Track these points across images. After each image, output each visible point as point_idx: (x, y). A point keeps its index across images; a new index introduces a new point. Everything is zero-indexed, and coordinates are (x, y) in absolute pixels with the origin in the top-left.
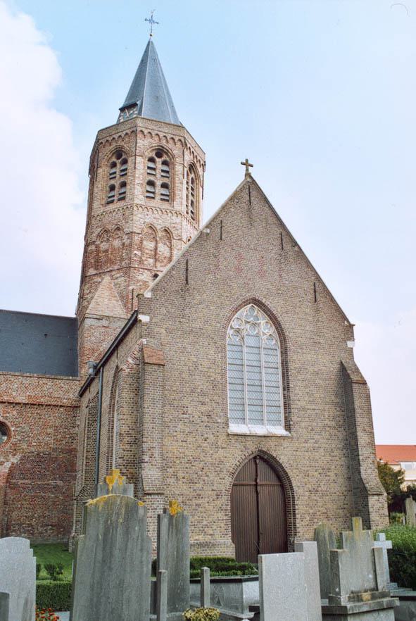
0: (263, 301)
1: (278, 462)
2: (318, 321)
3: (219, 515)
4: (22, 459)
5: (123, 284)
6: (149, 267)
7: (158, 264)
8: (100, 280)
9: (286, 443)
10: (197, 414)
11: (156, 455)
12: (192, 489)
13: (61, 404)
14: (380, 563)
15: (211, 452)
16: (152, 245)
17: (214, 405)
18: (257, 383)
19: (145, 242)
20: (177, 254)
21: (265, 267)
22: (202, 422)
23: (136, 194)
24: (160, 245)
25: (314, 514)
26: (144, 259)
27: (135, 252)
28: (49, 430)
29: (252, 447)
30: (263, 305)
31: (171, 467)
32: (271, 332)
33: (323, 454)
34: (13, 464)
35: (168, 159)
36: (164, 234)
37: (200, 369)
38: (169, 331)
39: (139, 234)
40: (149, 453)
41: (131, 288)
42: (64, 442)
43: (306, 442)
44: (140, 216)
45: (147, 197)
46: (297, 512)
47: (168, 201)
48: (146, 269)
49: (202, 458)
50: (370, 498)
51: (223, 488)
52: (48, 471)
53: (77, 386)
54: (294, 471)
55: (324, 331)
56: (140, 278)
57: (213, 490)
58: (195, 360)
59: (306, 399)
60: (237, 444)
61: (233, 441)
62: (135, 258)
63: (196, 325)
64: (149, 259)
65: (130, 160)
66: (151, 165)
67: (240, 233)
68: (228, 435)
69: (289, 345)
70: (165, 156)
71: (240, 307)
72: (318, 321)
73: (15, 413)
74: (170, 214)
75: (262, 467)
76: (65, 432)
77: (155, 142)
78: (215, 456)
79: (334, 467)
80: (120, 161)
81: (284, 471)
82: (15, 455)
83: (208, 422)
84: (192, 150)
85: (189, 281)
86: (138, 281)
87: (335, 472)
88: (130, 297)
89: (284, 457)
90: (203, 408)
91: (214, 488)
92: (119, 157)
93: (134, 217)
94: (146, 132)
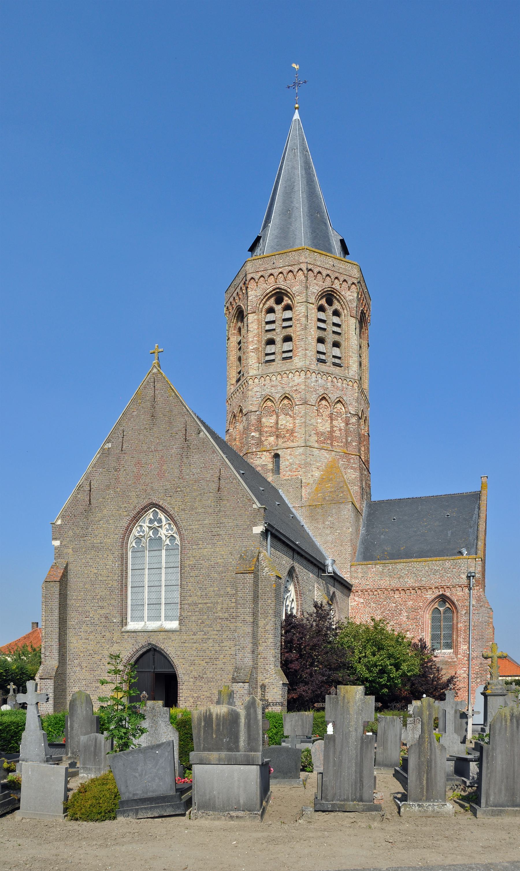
0: (160, 504)
2: (219, 511)
9: (174, 637)
10: (96, 617)
14: (488, 768)
15: (108, 646)
17: (111, 608)
18: (157, 584)
19: (264, 420)
22: (101, 623)
23: (251, 363)
25: (198, 697)
26: (263, 439)
27: (253, 434)
29: (142, 641)
31: (77, 659)
33: (211, 645)
35: (289, 302)
38: (75, 550)
39: (256, 411)
43: (194, 634)
44: (256, 389)
48: (264, 451)
49: (100, 652)
57: (108, 676)
58: (96, 571)
59: (198, 594)
60: (129, 639)
61: (126, 637)
62: (252, 442)
67: (141, 437)
70: (286, 298)
71: (137, 518)
72: (219, 511)
77: (269, 286)
79: (222, 656)
83: (106, 622)
87: (224, 661)
90: (102, 612)
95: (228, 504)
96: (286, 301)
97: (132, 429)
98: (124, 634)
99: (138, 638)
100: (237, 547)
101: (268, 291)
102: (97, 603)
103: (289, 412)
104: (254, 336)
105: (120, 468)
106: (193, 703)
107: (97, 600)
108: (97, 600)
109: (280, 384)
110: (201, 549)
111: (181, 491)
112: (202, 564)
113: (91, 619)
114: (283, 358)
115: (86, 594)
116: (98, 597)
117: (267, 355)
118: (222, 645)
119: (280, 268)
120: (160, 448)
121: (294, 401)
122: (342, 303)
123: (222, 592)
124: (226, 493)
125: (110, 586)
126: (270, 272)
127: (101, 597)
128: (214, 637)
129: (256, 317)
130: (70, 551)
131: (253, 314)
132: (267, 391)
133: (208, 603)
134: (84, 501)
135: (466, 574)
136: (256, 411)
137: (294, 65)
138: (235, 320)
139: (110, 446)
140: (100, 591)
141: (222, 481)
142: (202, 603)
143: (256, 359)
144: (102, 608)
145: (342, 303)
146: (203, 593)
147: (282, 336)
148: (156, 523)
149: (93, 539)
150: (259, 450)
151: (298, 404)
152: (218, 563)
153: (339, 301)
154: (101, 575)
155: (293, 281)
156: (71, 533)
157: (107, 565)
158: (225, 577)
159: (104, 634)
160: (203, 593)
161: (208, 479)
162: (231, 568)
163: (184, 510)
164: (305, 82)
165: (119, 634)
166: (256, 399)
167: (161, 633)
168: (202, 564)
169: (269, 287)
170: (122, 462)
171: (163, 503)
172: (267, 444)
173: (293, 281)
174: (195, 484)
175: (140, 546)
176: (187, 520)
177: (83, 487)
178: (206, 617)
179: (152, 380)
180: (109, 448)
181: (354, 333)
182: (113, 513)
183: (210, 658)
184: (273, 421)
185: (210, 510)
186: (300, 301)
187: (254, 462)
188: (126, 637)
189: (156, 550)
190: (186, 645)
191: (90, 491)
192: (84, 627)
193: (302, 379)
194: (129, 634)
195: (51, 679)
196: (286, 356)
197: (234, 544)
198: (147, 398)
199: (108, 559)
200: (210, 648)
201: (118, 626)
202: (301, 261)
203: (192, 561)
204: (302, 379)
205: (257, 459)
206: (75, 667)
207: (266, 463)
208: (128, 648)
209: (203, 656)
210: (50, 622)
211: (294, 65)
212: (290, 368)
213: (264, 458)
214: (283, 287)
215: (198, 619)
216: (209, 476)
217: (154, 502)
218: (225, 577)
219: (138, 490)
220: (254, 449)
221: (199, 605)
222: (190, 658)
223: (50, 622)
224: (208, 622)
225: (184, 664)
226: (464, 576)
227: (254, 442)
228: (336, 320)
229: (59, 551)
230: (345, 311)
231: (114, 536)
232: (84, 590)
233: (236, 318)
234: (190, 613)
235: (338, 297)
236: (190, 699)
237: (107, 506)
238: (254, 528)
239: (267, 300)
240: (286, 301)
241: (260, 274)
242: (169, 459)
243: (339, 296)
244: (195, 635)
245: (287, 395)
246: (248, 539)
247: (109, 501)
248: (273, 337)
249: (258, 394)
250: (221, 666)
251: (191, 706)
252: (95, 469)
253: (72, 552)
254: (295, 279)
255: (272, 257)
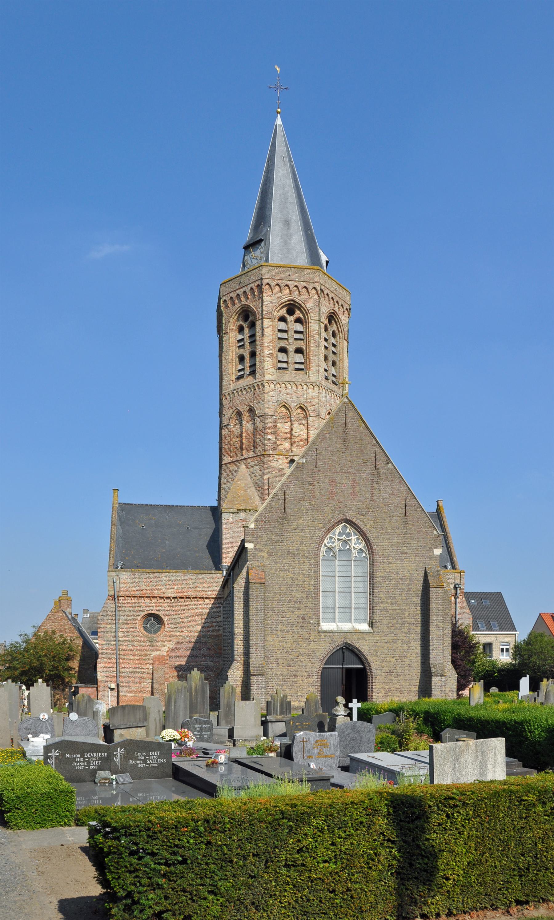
0: (354, 520)
1: (362, 653)
2: (406, 533)
3: (311, 689)
4: (176, 644)
5: (258, 473)
6: (284, 452)
7: (295, 448)
8: (236, 468)
9: (367, 637)
10: (293, 618)
11: (260, 648)
12: (289, 671)
13: (206, 596)
15: (305, 645)
16: (287, 426)
17: (308, 610)
19: (279, 425)
20: (313, 434)
21: (357, 489)
22: (298, 623)
23: (266, 367)
24: (296, 425)
25: (389, 689)
26: (278, 443)
27: (269, 437)
28: (198, 620)
29: (339, 641)
30: (354, 523)
31: (273, 656)
32: (361, 547)
33: (400, 645)
34: (169, 648)
35: (301, 316)
36: (299, 411)
37: (296, 582)
38: (270, 554)
39: (273, 416)
40: (255, 647)
41: (266, 477)
42: (211, 629)
44: (271, 394)
45: (279, 369)
46: (374, 687)
47: (302, 370)
48: (281, 455)
49: (297, 650)
50: (434, 679)
51: (314, 671)
52: (200, 654)
53: (219, 578)
54: (374, 658)
55: (411, 541)
56: (275, 465)
57: (305, 672)
58: (292, 575)
61: (323, 637)
62: (268, 444)
63: (292, 547)
64: (284, 443)
65: (258, 323)
66: (282, 326)
67: (334, 458)
68: (319, 632)
69: (377, 557)
72: (406, 533)
73: (166, 605)
74: (305, 387)
75: (347, 654)
76: (212, 621)
77: (285, 297)
78: (308, 647)
79: (409, 654)
80: (247, 323)
81: (366, 658)
82: (170, 641)
83: (303, 623)
84: (331, 295)
85: (287, 509)
86: (274, 469)
87: (411, 658)
88: (266, 487)
89: (364, 648)
91: (307, 670)
92: (246, 319)
93: (266, 396)
94: (273, 283)
95: (413, 528)
96: (298, 314)
97: (326, 449)
98: (321, 634)
99: (334, 637)
100: (421, 565)
101: (283, 301)
102: (293, 605)
103: (303, 422)
104: (270, 342)
105: (314, 483)
106: (385, 694)
107: (293, 602)
108: (293, 602)
109: (295, 394)
110: (391, 563)
111: (372, 512)
112: (391, 576)
113: (288, 619)
114: (296, 369)
115: (282, 596)
116: (295, 599)
117: (280, 362)
118: (409, 645)
119: (295, 281)
120: (353, 471)
121: (309, 413)
122: (339, 326)
123: (409, 601)
124: (411, 519)
125: (306, 590)
126: (286, 282)
127: (297, 600)
128: (402, 638)
129: (271, 323)
130: (265, 554)
131: (269, 320)
132: (283, 398)
133: (397, 610)
134: (279, 509)
135: (454, 585)
136: (273, 416)
137: (278, 69)
138: (236, 317)
139: (304, 462)
140: (296, 594)
141: (407, 508)
142: (392, 610)
143: (272, 364)
144: (299, 609)
145: (339, 326)
146: (393, 601)
147: (294, 347)
148: (344, 536)
149: (288, 545)
150: (276, 454)
151: (312, 415)
152: (405, 577)
153: (336, 324)
154: (297, 579)
155: (307, 297)
156: (265, 537)
157: (303, 571)
158: (411, 588)
159: (301, 633)
160: (393, 601)
161: (396, 505)
162: (416, 582)
163: (375, 528)
164: (287, 89)
165: (316, 634)
166: (272, 404)
167: (356, 634)
168: (391, 576)
169: (284, 297)
170: (317, 478)
171: (356, 521)
172: (282, 448)
173: (307, 297)
174: (384, 507)
175: (330, 556)
176: (378, 537)
177: (277, 495)
178: (395, 621)
179: (344, 408)
180: (303, 463)
181: (346, 355)
182: (309, 524)
183: (399, 656)
184: (288, 428)
185: (399, 532)
186: (314, 319)
187: (271, 464)
188: (323, 637)
189: (343, 560)
190: (378, 644)
191: (285, 500)
192: (280, 626)
193: (316, 393)
194: (326, 634)
195: (263, 675)
196: (298, 368)
197: (419, 562)
198: (339, 424)
199: (304, 566)
200: (400, 648)
201: (315, 627)
202: (316, 281)
203: (383, 573)
204: (316, 393)
205: (273, 461)
206: (271, 663)
207: (283, 467)
208: (325, 647)
209: (393, 654)
210: (255, 621)
211: (278, 69)
212: (304, 380)
213: (281, 462)
214: (297, 300)
215: (389, 623)
216: (396, 502)
217: (348, 518)
218: (411, 588)
219: (332, 505)
220: (271, 452)
221: (390, 611)
222: (382, 656)
223: (255, 621)
224: (397, 626)
225: (376, 661)
226: (452, 587)
227: (270, 445)
228: (299, 327)
229: (252, 553)
230: (341, 334)
231: (310, 545)
232: (280, 592)
233: (237, 315)
234: (382, 618)
235: (336, 319)
236: (382, 690)
237: (302, 517)
238: (435, 550)
239: (281, 309)
240: (298, 314)
241: (276, 282)
242: (361, 482)
243: (338, 319)
244: (386, 636)
245: (302, 406)
246: (430, 559)
247: (304, 512)
248: (286, 346)
249: (274, 398)
250: (409, 663)
251: (383, 697)
252: (289, 480)
253: (267, 555)
254: (309, 296)
255: (288, 268)
